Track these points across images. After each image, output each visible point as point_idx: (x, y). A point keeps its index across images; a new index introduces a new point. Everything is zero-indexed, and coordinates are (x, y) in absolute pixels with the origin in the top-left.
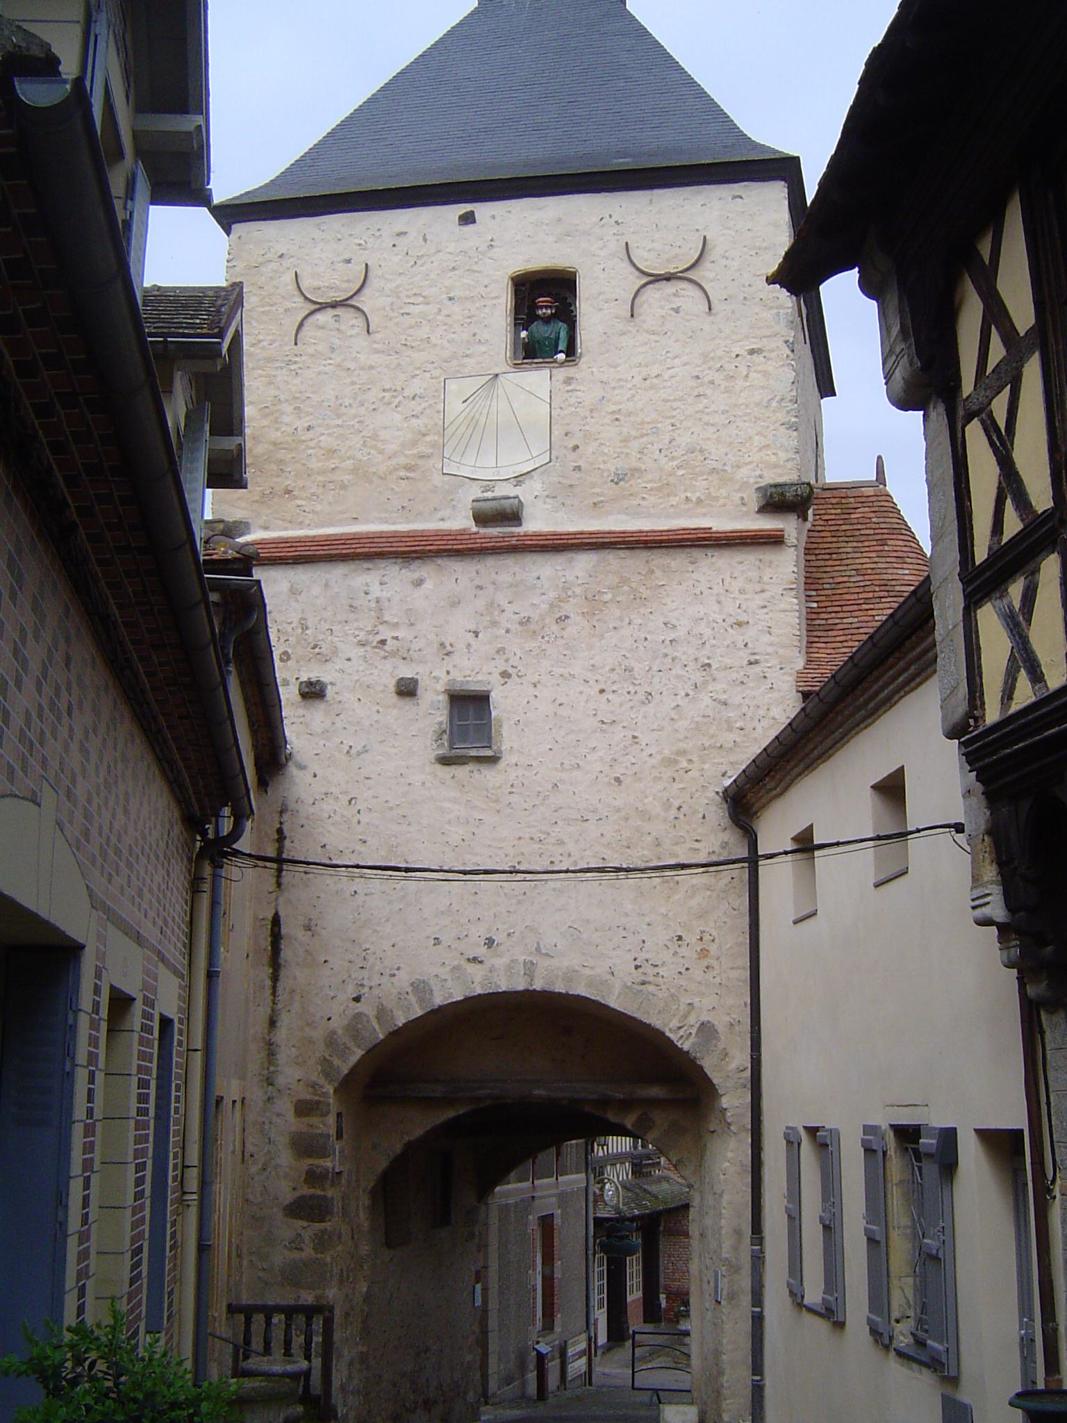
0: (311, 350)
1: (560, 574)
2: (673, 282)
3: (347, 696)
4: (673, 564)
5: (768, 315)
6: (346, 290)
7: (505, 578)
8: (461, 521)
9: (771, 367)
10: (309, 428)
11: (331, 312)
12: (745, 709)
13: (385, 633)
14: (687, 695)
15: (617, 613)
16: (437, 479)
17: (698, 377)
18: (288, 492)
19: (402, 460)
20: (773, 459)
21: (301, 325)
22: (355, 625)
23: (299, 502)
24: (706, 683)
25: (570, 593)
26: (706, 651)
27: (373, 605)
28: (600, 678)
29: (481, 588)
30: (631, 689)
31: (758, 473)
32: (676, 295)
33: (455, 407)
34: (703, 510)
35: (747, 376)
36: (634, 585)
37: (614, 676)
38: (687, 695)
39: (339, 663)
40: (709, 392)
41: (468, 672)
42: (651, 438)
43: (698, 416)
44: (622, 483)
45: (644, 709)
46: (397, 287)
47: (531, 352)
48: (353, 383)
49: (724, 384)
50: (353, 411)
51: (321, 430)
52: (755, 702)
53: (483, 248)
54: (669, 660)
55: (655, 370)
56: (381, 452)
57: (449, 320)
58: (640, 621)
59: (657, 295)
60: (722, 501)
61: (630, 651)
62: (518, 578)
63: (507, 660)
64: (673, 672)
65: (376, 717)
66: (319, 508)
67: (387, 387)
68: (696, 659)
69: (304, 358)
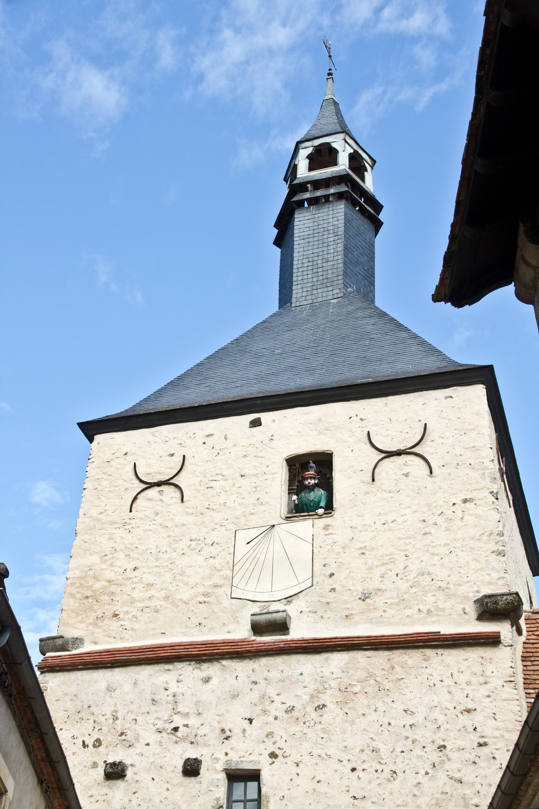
0: (141, 515)
1: (319, 670)
2: (403, 456)
3: (144, 777)
4: (410, 662)
5: (476, 475)
6: (169, 474)
7: (275, 674)
8: (241, 632)
9: (479, 511)
10: (135, 569)
11: (157, 489)
12: (478, 787)
13: (178, 721)
14: (427, 773)
15: (365, 702)
16: (227, 602)
17: (424, 521)
18: (116, 615)
19: (202, 590)
20: (488, 578)
21: (135, 498)
22: (156, 715)
23: (122, 623)
24: (442, 762)
25: (326, 686)
26: (442, 734)
27: (171, 698)
28: (351, 758)
29: (255, 683)
30: (379, 768)
31: (476, 589)
32: (406, 464)
33: (242, 549)
34: (434, 619)
35: (462, 518)
36: (378, 679)
37: (364, 756)
38: (427, 773)
39: (140, 747)
40: (433, 531)
41: (243, 754)
42: (390, 566)
43: (426, 549)
44: (367, 600)
45: (390, 786)
46: (205, 470)
47: (300, 510)
48: (169, 536)
49: (445, 525)
50: (167, 556)
51: (144, 570)
52: (487, 781)
53: (266, 441)
54: (410, 742)
55: (391, 518)
56: (187, 584)
57: (240, 490)
58: (384, 709)
59: (392, 465)
60: (448, 612)
61: (377, 734)
62: (285, 674)
63: (274, 743)
64: (414, 753)
65: (166, 794)
66: (136, 626)
67: (193, 538)
68: (433, 742)
69: (135, 521)
